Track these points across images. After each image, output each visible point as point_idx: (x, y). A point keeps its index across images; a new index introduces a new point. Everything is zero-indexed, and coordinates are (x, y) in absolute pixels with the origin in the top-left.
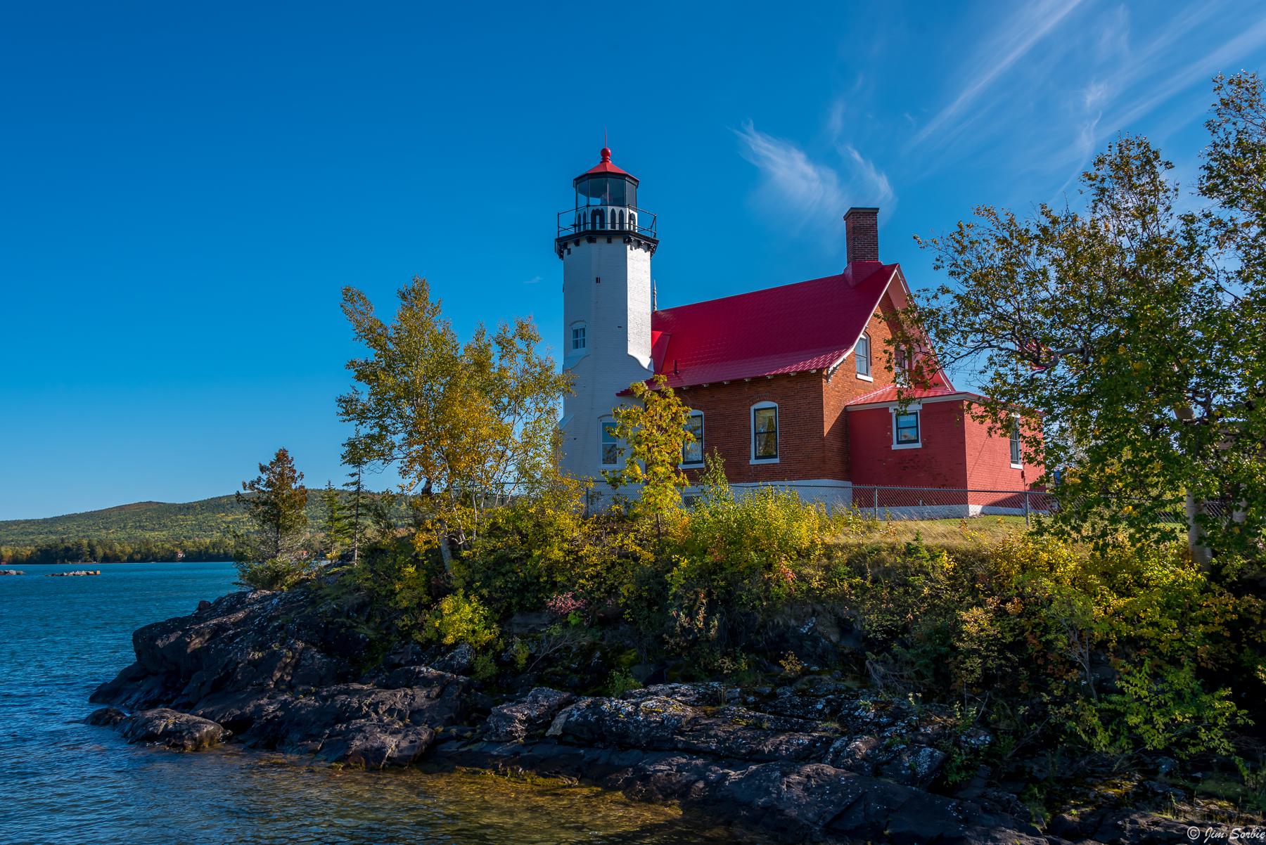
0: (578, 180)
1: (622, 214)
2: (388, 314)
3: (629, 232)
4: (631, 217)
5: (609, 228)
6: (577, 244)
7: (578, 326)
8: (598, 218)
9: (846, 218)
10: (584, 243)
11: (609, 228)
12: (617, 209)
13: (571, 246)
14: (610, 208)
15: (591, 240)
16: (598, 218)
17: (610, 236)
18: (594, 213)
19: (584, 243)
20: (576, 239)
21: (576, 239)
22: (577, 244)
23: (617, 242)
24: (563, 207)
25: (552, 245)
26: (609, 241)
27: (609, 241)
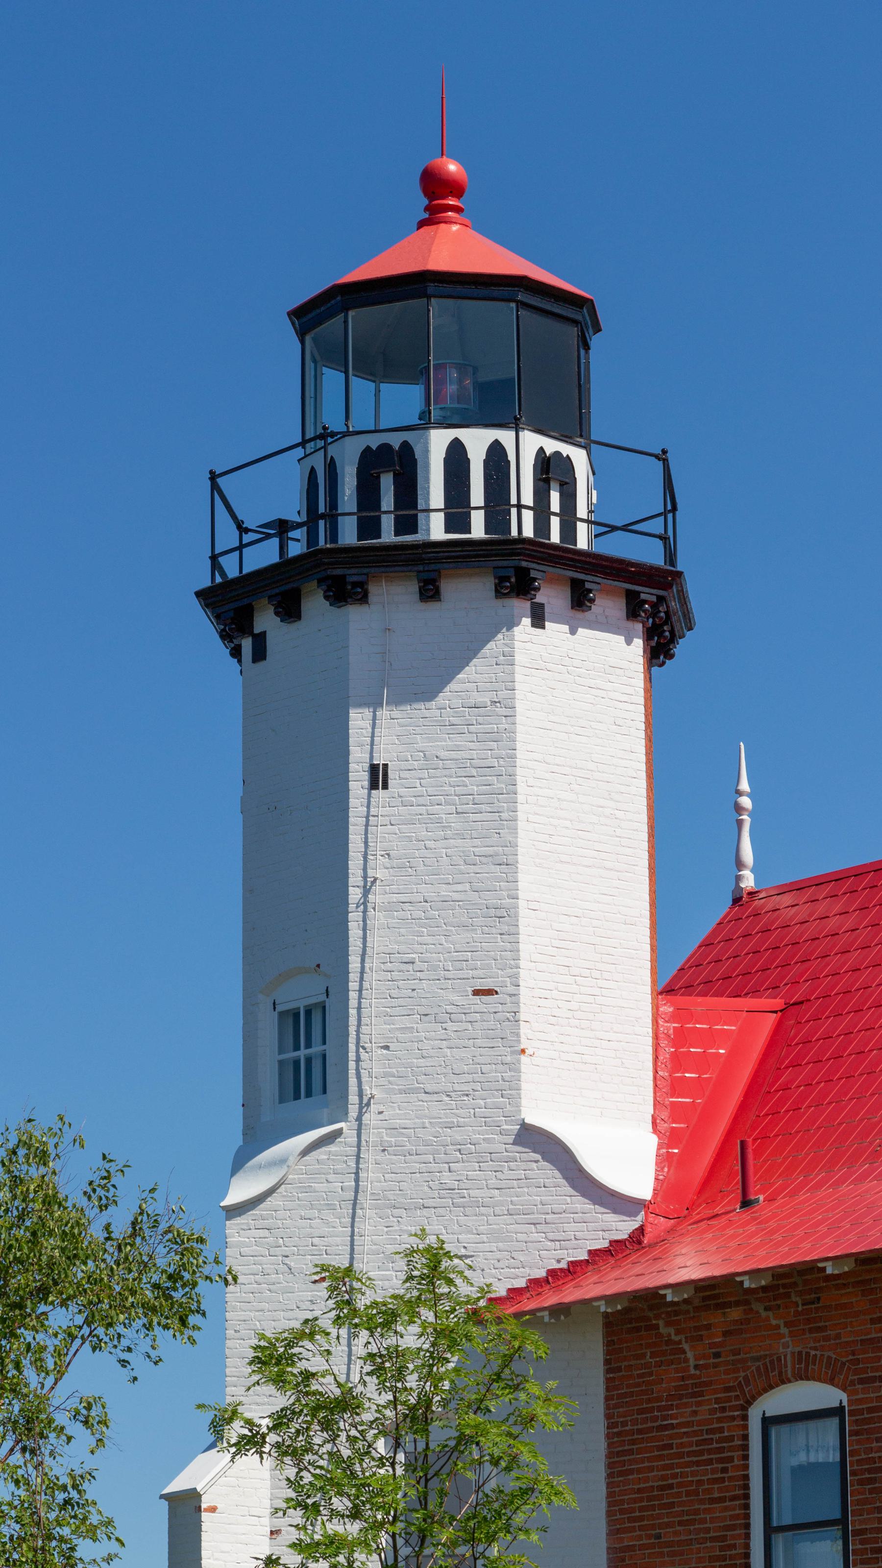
0: (307, 317)
1: (497, 461)
2: (262, 1404)
3: (537, 550)
4: (550, 469)
5: (436, 529)
6: (290, 610)
7: (300, 994)
8: (387, 483)
9: (363, 599)
10: (315, 604)
11: (436, 529)
12: (477, 441)
13: (266, 620)
14: (439, 441)
15: (346, 592)
16: (387, 483)
17: (429, 569)
18: (372, 463)
19: (315, 604)
20: (283, 589)
21: (283, 589)
22: (290, 610)
23: (467, 593)
24: (249, 430)
25: (203, 628)
26: (430, 592)
27: (430, 592)
